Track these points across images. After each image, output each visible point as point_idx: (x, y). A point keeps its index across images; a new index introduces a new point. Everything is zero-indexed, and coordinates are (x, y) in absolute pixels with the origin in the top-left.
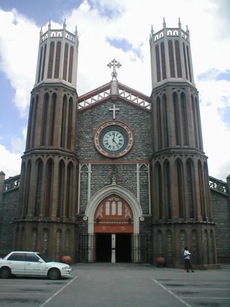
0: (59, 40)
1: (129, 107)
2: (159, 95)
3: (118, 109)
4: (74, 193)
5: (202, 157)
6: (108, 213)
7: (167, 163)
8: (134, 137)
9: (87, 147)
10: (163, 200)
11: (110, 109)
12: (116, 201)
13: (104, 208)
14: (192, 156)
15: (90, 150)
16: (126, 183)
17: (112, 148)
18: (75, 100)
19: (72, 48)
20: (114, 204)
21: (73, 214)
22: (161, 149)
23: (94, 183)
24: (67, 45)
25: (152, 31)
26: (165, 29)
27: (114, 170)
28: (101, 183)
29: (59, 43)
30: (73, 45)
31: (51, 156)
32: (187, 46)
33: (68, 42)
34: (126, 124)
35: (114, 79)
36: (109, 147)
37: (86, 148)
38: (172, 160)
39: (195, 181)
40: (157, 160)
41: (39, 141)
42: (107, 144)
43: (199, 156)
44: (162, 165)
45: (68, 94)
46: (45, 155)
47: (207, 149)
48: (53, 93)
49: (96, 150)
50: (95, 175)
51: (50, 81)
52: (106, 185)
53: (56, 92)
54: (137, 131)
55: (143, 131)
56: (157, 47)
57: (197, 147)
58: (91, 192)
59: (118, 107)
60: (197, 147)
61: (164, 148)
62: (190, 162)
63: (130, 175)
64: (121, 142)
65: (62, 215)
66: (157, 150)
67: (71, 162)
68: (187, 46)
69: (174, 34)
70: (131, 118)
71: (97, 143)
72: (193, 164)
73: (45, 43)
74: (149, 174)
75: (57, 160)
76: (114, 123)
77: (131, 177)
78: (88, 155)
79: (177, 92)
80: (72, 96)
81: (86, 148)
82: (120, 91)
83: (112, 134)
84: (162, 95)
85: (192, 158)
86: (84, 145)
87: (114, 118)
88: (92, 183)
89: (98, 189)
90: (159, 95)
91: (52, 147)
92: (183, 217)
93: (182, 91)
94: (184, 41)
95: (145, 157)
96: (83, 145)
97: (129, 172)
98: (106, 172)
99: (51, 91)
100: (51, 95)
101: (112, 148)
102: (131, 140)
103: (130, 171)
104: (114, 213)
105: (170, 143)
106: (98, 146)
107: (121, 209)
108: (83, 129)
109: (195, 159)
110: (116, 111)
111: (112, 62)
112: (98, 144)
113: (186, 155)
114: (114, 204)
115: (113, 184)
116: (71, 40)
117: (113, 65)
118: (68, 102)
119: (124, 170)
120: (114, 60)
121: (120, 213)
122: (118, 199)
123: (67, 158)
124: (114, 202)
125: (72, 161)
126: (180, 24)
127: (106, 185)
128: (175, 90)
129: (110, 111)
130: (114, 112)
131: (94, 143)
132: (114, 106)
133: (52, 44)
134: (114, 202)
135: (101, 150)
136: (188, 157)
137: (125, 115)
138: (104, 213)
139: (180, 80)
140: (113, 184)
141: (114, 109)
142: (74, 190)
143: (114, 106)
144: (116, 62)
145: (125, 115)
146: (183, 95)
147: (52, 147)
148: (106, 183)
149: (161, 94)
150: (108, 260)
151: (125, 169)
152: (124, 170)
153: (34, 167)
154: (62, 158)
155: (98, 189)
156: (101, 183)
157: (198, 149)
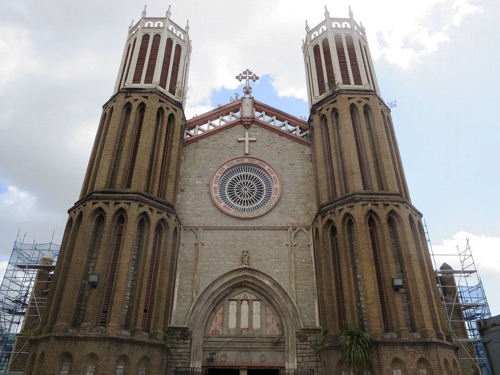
0: (157, 32)
4: (166, 280)
6: (232, 324)
7: (349, 221)
8: (282, 184)
10: (346, 293)
13: (225, 315)
14: (397, 206)
18: (178, 122)
19: (179, 48)
20: (245, 307)
21: (160, 324)
22: (333, 200)
24: (170, 42)
25: (307, 27)
26: (328, 20)
28: (221, 263)
29: (157, 37)
30: (181, 43)
31: (122, 205)
33: (172, 36)
35: (247, 96)
38: (359, 212)
39: (409, 256)
40: (328, 216)
41: (105, 179)
43: (410, 208)
44: (339, 225)
45: (168, 109)
46: (112, 203)
47: (417, 199)
48: (138, 102)
49: (215, 205)
53: (144, 100)
56: (316, 49)
61: (339, 196)
62: (392, 218)
65: (135, 324)
66: (325, 200)
67: (163, 220)
69: (344, 26)
71: (216, 193)
72: (401, 221)
74: (312, 247)
75: (134, 211)
76: (246, 161)
78: (199, 213)
79: (356, 103)
80: (174, 112)
82: (257, 114)
84: (330, 111)
85: (396, 209)
87: (247, 152)
91: (128, 190)
92: (393, 330)
93: (365, 102)
99: (136, 100)
100: (135, 106)
102: (277, 189)
104: (244, 324)
106: (217, 197)
107: (259, 316)
109: (403, 212)
111: (245, 73)
112: (218, 195)
113: (386, 205)
114: (245, 307)
116: (178, 35)
117: (245, 78)
118: (166, 120)
120: (248, 70)
121: (257, 325)
122: (254, 297)
123: (155, 210)
124: (245, 302)
125: (166, 217)
126: (351, 14)
128: (354, 101)
129: (240, 142)
130: (247, 142)
131: (210, 194)
132: (247, 134)
133: (146, 37)
134: (245, 302)
135: (223, 204)
136: (389, 209)
142: (167, 274)
143: (247, 134)
144: (250, 73)
146: (367, 108)
147: (128, 190)
150: (323, 114)
151: (267, 238)
153: (89, 224)
154: (146, 208)
156: (221, 263)
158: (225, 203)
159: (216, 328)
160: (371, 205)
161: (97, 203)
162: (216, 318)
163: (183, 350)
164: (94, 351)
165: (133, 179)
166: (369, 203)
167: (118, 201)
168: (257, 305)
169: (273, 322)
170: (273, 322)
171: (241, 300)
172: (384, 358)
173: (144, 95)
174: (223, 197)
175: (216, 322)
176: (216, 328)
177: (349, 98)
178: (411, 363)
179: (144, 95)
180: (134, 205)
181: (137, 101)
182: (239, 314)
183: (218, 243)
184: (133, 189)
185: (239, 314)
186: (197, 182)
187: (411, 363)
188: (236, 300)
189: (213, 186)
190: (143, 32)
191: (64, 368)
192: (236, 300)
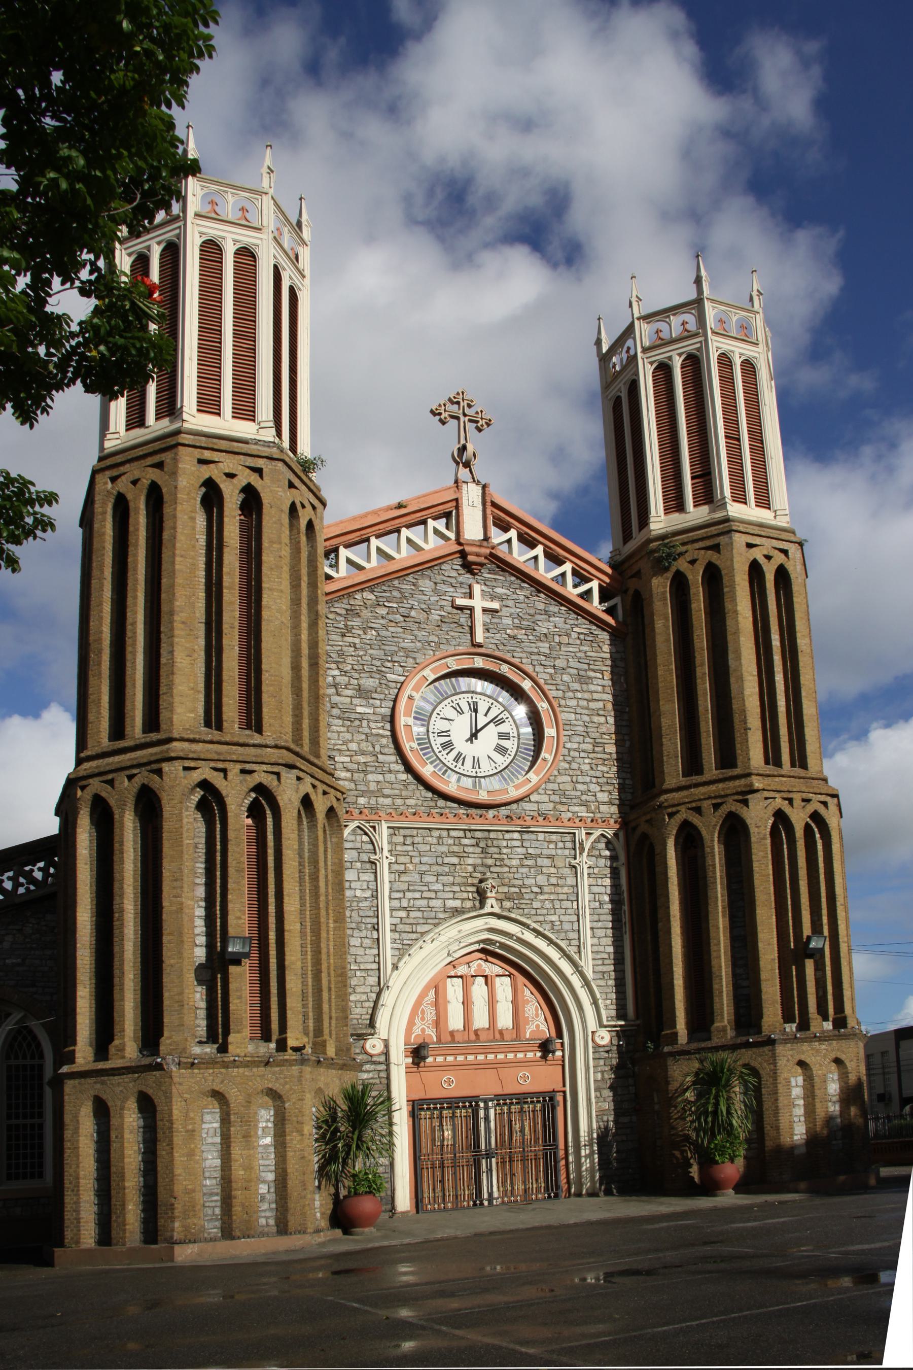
1: (540, 602)
2: (123, 485)
3: (495, 605)
5: (321, 787)
6: (455, 1021)
9: (363, 753)
11: (460, 602)
12: (486, 977)
15: (380, 768)
16: (536, 904)
17: (469, 763)
20: (479, 989)
23: (405, 903)
27: (484, 851)
28: (433, 903)
32: (292, 290)
34: (529, 669)
36: (456, 759)
37: (362, 759)
42: (448, 746)
50: (404, 872)
51: (678, 521)
52: (457, 912)
54: (573, 703)
55: (593, 705)
57: (298, 739)
58: (394, 941)
59: (493, 598)
60: (298, 739)
63: (548, 875)
64: (504, 743)
68: (292, 290)
70: (544, 647)
73: (627, 377)
77: (553, 880)
78: (373, 786)
79: (762, 561)
81: (362, 759)
82: (497, 537)
83: (465, 708)
86: (353, 746)
88: (396, 904)
89: (420, 929)
90: (123, 485)
94: (284, 262)
95: (603, 808)
96: (345, 743)
97: (547, 862)
98: (455, 860)
101: (469, 763)
103: (550, 857)
104: (480, 1020)
105: (164, 715)
108: (344, 673)
110: (485, 610)
115: (487, 909)
119: (527, 856)
121: (505, 1020)
122: (497, 970)
127: (457, 912)
129: (461, 608)
130: (478, 613)
132: (477, 589)
137: (521, 634)
138: (439, 1023)
139: (244, 429)
140: (487, 909)
141: (478, 603)
145: (521, 634)
148: (457, 904)
149: (693, 562)
152: (527, 856)
155: (420, 929)
156: (433, 903)
157: (306, 749)
158: (435, 767)
159: (423, 1030)
160: (780, 800)
161: (195, 768)
162: (423, 1012)
163: (371, 1075)
164: (270, 1086)
165: (265, 710)
166: (777, 795)
167: (248, 767)
168: (504, 987)
169: (537, 1015)
170: (537, 1015)
171: (473, 976)
172: (781, 1062)
173: (251, 462)
174: (517, 771)
175: (423, 1019)
176: (423, 1030)
177: (750, 546)
178: (821, 1065)
179: (251, 462)
180: (289, 776)
181: (235, 481)
182: (467, 1003)
183: (424, 860)
184: (268, 736)
185: (467, 1003)
186: (360, 709)
187: (821, 1065)
188: (461, 977)
189: (403, 723)
190: (201, 234)
191: (207, 1118)
192: (461, 977)
